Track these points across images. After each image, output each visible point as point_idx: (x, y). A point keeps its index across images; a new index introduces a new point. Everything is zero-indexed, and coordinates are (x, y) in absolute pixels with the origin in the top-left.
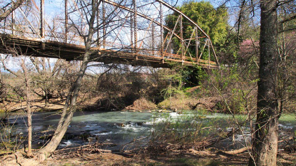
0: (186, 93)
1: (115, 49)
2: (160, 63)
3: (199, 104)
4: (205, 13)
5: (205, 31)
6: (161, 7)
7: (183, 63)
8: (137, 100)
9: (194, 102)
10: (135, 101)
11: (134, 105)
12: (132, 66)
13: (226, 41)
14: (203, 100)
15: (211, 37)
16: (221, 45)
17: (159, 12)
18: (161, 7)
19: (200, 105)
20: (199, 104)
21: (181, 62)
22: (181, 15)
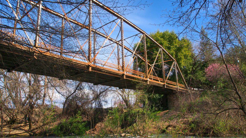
0: (141, 46)
1: (50, 44)
2: (121, 78)
3: (169, 126)
4: (169, 41)
5: (172, 55)
6: (121, 23)
7: (148, 82)
8: (100, 123)
9: (163, 124)
10: (98, 124)
11: (96, 129)
12: (94, 85)
13: (192, 68)
14: (173, 123)
15: (178, 60)
16: (189, 72)
17: (120, 27)
18: (121, 23)
19: (170, 128)
20: (169, 126)
21: (147, 80)
22: (145, 35)
